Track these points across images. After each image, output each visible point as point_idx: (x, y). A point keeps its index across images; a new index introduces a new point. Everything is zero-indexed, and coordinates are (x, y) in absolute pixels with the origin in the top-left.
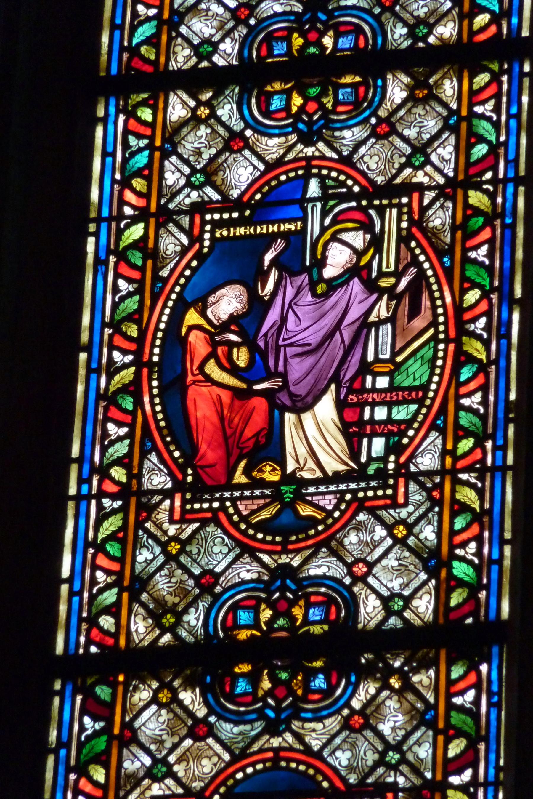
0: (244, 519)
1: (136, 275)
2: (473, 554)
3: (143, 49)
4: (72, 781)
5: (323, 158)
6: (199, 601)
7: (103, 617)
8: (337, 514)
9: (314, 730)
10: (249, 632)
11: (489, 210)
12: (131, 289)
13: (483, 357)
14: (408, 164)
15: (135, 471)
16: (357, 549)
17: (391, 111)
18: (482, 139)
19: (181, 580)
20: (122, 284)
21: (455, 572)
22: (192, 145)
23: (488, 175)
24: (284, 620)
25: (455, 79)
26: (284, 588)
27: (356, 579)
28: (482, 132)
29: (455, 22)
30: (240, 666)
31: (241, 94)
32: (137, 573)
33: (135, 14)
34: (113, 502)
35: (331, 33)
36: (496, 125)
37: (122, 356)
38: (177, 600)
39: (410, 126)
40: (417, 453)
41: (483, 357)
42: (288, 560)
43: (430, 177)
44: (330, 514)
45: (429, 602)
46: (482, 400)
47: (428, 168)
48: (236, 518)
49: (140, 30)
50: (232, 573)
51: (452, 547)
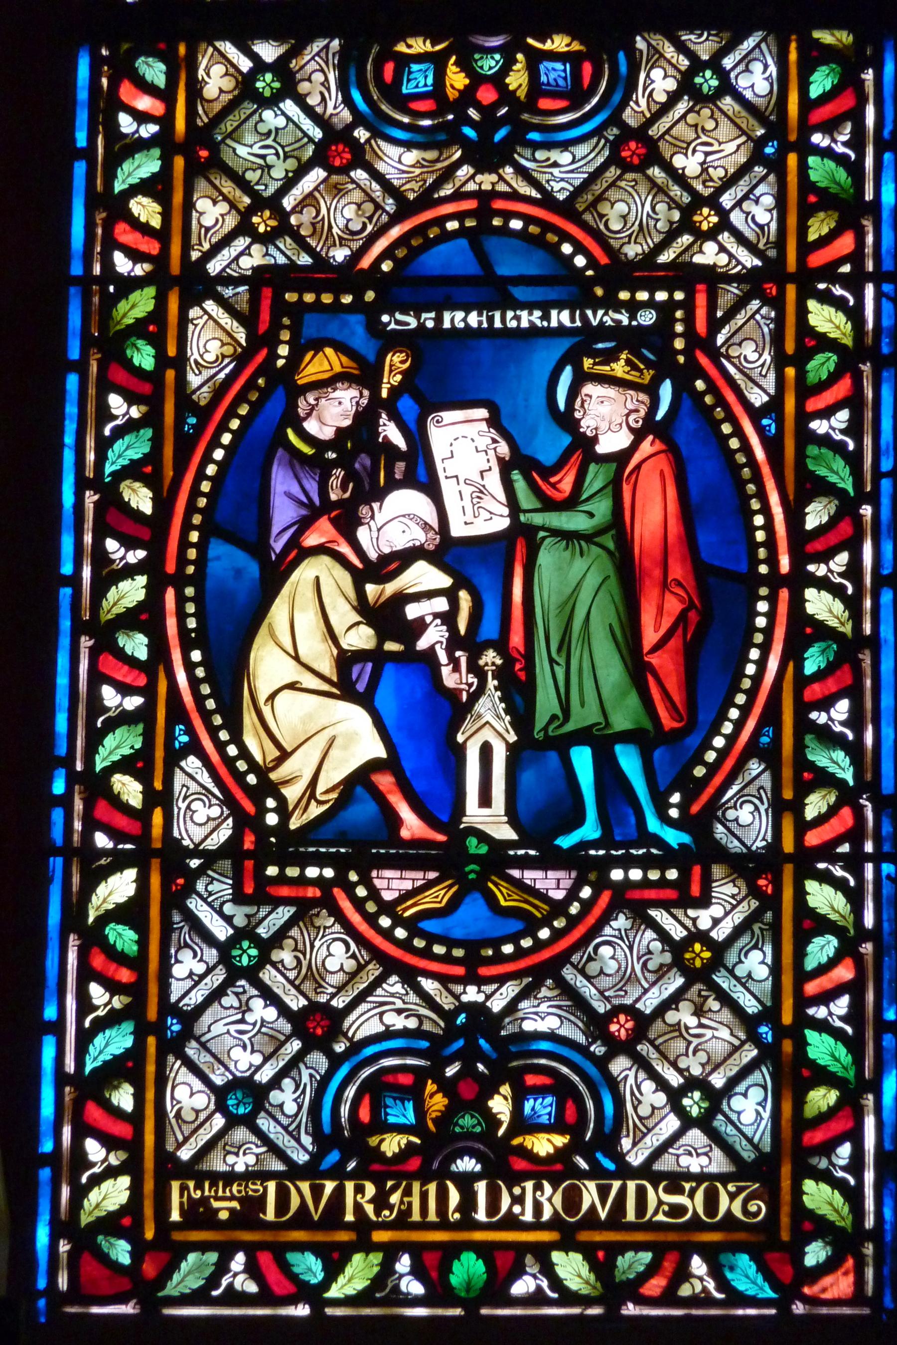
0: (387, 908)
1: (125, 975)
2: (841, 1018)
4: (65, 1255)
5: (514, 196)
6: (302, 1066)
7: (112, 925)
8: (574, 909)
9: (555, 165)
10: (548, 46)
11: (848, 341)
12: (135, 412)
13: (848, 485)
14: (686, 225)
15: (172, 351)
16: (616, 985)
17: (648, 115)
19: (263, 1021)
20: (97, 992)
21: (812, 1053)
22: (249, 150)
24: (473, 1117)
25: (770, 61)
26: (469, 1056)
27: (616, 1047)
28: (822, 472)
29: (765, 1088)
30: (410, 41)
31: (343, 53)
32: (173, 998)
33: (101, 558)
34: (127, 551)
35: (505, 1089)
36: (854, 461)
37: (123, 550)
38: (257, 1059)
39: (687, 149)
40: (723, 801)
41: (848, 485)
42: (481, 998)
43: (731, 256)
44: (559, 908)
45: (761, 1104)
46: (849, 716)
47: (725, 237)
48: (371, 907)
49: (110, 741)
50: (365, 1013)
51: (802, 1002)
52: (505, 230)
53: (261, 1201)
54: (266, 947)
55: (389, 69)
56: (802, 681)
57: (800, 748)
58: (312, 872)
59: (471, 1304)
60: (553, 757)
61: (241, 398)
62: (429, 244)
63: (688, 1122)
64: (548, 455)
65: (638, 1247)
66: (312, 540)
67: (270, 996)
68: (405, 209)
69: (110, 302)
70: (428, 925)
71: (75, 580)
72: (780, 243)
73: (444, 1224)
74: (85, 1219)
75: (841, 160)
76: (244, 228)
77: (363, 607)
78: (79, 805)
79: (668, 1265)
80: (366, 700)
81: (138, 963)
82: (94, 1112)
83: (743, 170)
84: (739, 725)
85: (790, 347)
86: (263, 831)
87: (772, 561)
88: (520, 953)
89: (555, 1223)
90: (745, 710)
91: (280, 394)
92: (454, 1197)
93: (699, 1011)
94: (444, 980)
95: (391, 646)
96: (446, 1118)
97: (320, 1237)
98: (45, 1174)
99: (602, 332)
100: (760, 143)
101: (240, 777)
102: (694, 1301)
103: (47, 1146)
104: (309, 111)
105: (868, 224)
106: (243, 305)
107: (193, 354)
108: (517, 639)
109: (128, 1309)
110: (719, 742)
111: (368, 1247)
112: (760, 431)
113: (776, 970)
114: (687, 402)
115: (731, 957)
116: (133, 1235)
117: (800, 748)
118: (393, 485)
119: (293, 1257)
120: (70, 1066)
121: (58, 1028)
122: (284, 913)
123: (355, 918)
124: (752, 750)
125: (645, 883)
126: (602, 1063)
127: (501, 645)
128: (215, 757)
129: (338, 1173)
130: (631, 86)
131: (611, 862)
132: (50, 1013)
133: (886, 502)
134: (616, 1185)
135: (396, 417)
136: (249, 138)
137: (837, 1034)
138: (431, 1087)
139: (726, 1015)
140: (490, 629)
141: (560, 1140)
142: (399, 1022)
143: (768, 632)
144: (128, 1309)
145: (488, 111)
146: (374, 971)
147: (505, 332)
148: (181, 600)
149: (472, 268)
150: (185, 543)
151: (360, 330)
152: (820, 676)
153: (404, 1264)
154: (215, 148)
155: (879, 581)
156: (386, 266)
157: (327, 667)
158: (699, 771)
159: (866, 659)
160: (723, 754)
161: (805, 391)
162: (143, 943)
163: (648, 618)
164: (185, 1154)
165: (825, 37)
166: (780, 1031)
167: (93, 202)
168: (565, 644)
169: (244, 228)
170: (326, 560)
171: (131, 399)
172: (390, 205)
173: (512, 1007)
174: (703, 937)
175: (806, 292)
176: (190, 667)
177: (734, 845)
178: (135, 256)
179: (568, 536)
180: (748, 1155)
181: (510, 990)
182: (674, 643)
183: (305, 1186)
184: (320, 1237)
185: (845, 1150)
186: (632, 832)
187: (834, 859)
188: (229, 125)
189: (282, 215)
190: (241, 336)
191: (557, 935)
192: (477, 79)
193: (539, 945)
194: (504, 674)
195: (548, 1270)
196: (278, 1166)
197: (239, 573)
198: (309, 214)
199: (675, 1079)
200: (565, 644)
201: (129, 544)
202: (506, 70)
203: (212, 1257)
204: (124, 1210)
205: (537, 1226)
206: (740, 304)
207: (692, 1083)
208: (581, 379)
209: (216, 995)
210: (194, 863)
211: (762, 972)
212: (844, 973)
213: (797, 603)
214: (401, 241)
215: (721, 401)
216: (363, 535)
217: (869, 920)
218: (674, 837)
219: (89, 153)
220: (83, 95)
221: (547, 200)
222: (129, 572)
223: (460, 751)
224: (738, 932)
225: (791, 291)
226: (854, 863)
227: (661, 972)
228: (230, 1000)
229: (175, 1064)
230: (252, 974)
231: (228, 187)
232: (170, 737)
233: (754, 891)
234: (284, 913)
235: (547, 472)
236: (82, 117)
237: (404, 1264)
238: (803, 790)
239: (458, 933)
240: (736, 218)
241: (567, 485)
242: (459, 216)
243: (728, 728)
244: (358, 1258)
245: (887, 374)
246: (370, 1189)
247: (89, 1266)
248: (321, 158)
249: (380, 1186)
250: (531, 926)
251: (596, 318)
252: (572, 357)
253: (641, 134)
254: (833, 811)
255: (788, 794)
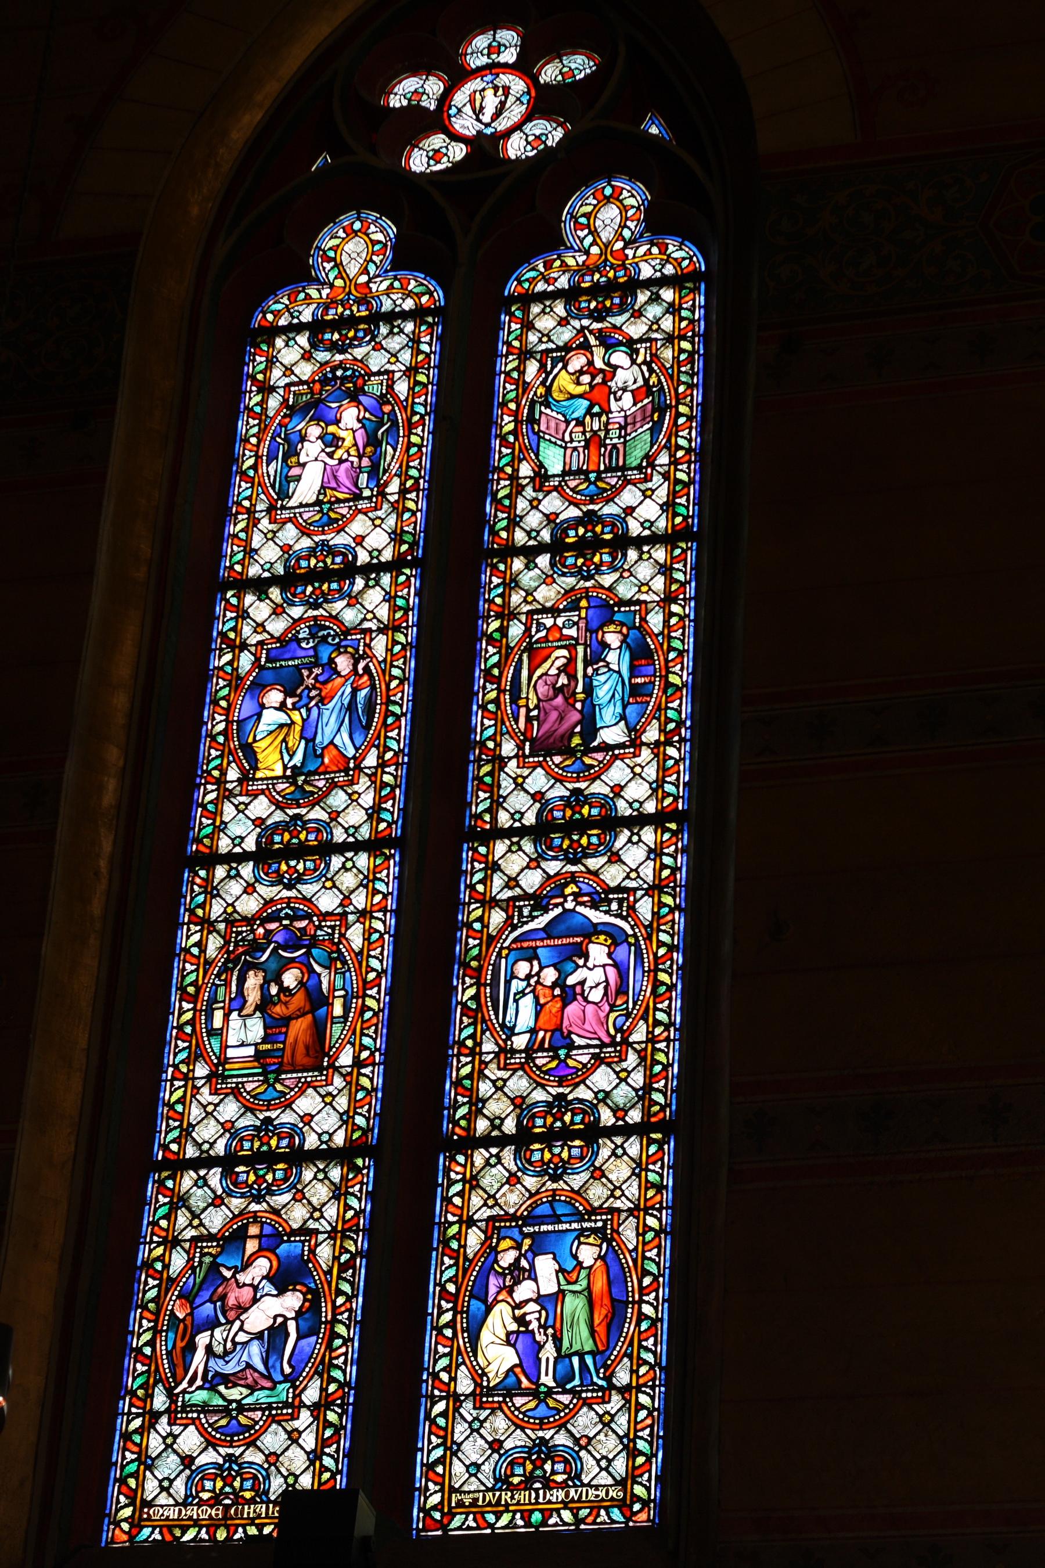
0: (517, 1409)
1: (442, 1433)
3: (469, 1003)
5: (563, 1190)
8: (571, 1406)
11: (658, 1228)
13: (656, 1272)
18: (679, 515)
20: (433, 1438)
21: (638, 1446)
23: (682, 596)
27: (582, 1448)
28: (648, 1268)
31: (515, 1150)
33: (440, 1306)
35: (549, 1462)
36: (658, 1264)
41: (656, 1272)
44: (567, 1406)
47: (623, 1198)
48: (513, 1409)
49: (440, 1362)
52: (560, 1200)
53: (477, 1499)
54: (482, 1422)
55: (528, 1153)
56: (640, 1333)
57: (639, 1353)
58: (496, 1399)
59: (537, 1527)
60: (567, 1360)
61: (482, 1256)
62: (538, 1206)
63: (601, 1469)
64: (569, 1269)
65: (585, 1508)
66: (500, 1298)
67: (482, 1437)
68: (532, 1195)
69: (446, 1229)
70: (529, 1414)
71: (432, 1314)
72: (639, 1200)
73: (530, 1504)
74: (428, 1507)
75: (657, 1173)
76: (485, 1204)
77: (514, 1318)
78: (430, 1382)
79: (594, 1513)
80: (514, 1346)
81: (445, 1429)
82: (431, 1475)
83: (629, 1178)
84: (621, 1347)
85: (641, 1231)
86: (482, 1387)
87: (633, 1296)
88: (555, 1420)
89: (562, 1502)
90: (623, 1343)
91: (493, 1253)
92: (533, 1495)
93: (606, 1436)
94: (533, 1430)
95: (522, 1329)
96: (532, 1472)
97: (494, 1509)
98: (417, 1493)
99: (587, 1229)
100: (634, 1169)
101: (476, 1371)
102: (601, 1523)
103: (418, 1485)
104: (505, 1168)
105: (664, 1192)
106: (484, 1228)
107: (468, 1243)
108: (558, 1325)
109: (439, 1533)
110: (615, 1353)
111: (508, 1511)
112: (631, 1256)
113: (629, 1422)
114: (610, 1249)
115: (616, 1419)
116: (441, 1511)
117: (639, 1353)
118: (524, 1279)
119: (486, 1515)
120: (425, 1461)
121: (422, 1450)
122: (488, 1412)
123: (508, 1412)
124: (625, 1355)
125: (592, 1397)
126: (577, 1453)
127: (553, 1327)
128: (469, 1365)
129: (500, 1489)
130: (597, 1154)
131: (582, 1391)
132: (420, 1445)
133: (667, 1276)
134: (580, 1489)
135: (526, 1258)
136: (487, 1177)
137: (646, 1440)
138: (528, 1462)
139: (614, 1436)
140: (550, 1322)
141: (565, 1477)
142: (519, 1443)
143: (631, 1319)
144: (439, 1533)
145: (556, 1165)
146: (513, 1428)
147: (559, 1231)
148: (462, 1318)
149: (550, 1212)
150: (464, 1301)
151: (517, 1233)
152: (646, 1331)
153: (518, 1516)
154: (478, 1181)
155: (664, 1300)
156: (525, 1213)
157: (504, 1337)
158: (609, 1362)
159: (659, 1325)
160: (616, 1356)
161: (644, 1243)
162: (447, 1423)
163: (596, 1316)
164: (457, 1486)
165: (653, 1136)
166: (629, 1440)
167: (443, 1199)
168: (572, 1325)
169: (485, 1204)
170: (504, 1304)
171: (451, 1258)
172: (527, 1195)
173: (552, 1437)
174: (608, 1413)
175: (646, 1213)
176: (463, 1338)
177: (618, 1385)
178: (454, 1215)
179: (574, 1292)
180: (619, 1478)
181: (552, 1431)
182: (604, 1323)
183: (491, 1494)
184: (494, 1509)
185: (646, 1476)
186: (589, 1382)
187: (647, 1387)
188: (482, 1174)
189: (496, 1200)
190: (483, 1236)
191: (566, 1414)
192: (553, 1155)
193: (561, 1418)
194: (553, 1335)
195: (559, 1516)
196: (483, 1488)
197: (479, 1309)
198: (504, 1199)
199: (598, 1457)
200: (572, 1325)
201: (448, 1302)
202: (561, 1152)
203: (464, 1516)
204: (439, 1503)
205: (557, 1503)
206: (627, 1218)
207: (604, 1457)
208: (580, 1243)
209: (467, 1438)
210: (462, 1398)
211: (625, 1423)
212: (649, 1421)
213: (640, 1308)
214: (530, 1205)
215: (620, 1248)
216: (514, 1295)
217: (656, 1406)
218: (601, 1382)
219: (442, 1185)
220: (441, 1168)
221: (572, 1190)
222: (447, 1310)
223: (540, 1360)
224: (619, 1411)
225: (642, 1213)
226: (653, 1388)
227: (596, 1424)
228: (471, 1439)
229: (455, 1459)
230: (477, 1431)
231: (481, 1192)
232: (457, 1360)
233: (624, 1398)
234: (488, 1412)
235: (569, 1273)
236: (441, 1174)
237: (518, 1516)
238: (639, 1366)
239: (537, 1416)
240: (627, 1193)
241: (574, 1277)
242: (547, 1197)
243: (618, 1348)
244: (505, 1515)
245: (669, 1237)
246: (509, 1494)
247: (428, 1521)
248: (508, 1182)
249: (512, 1492)
250: (559, 1411)
251: (586, 1225)
252: (578, 1238)
253: (600, 1169)
254: (647, 1372)
255: (635, 1368)
